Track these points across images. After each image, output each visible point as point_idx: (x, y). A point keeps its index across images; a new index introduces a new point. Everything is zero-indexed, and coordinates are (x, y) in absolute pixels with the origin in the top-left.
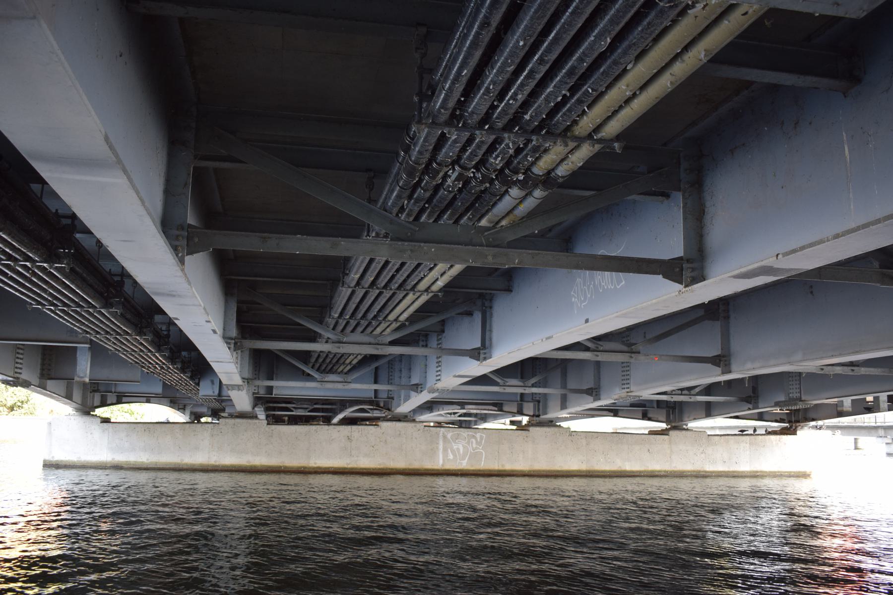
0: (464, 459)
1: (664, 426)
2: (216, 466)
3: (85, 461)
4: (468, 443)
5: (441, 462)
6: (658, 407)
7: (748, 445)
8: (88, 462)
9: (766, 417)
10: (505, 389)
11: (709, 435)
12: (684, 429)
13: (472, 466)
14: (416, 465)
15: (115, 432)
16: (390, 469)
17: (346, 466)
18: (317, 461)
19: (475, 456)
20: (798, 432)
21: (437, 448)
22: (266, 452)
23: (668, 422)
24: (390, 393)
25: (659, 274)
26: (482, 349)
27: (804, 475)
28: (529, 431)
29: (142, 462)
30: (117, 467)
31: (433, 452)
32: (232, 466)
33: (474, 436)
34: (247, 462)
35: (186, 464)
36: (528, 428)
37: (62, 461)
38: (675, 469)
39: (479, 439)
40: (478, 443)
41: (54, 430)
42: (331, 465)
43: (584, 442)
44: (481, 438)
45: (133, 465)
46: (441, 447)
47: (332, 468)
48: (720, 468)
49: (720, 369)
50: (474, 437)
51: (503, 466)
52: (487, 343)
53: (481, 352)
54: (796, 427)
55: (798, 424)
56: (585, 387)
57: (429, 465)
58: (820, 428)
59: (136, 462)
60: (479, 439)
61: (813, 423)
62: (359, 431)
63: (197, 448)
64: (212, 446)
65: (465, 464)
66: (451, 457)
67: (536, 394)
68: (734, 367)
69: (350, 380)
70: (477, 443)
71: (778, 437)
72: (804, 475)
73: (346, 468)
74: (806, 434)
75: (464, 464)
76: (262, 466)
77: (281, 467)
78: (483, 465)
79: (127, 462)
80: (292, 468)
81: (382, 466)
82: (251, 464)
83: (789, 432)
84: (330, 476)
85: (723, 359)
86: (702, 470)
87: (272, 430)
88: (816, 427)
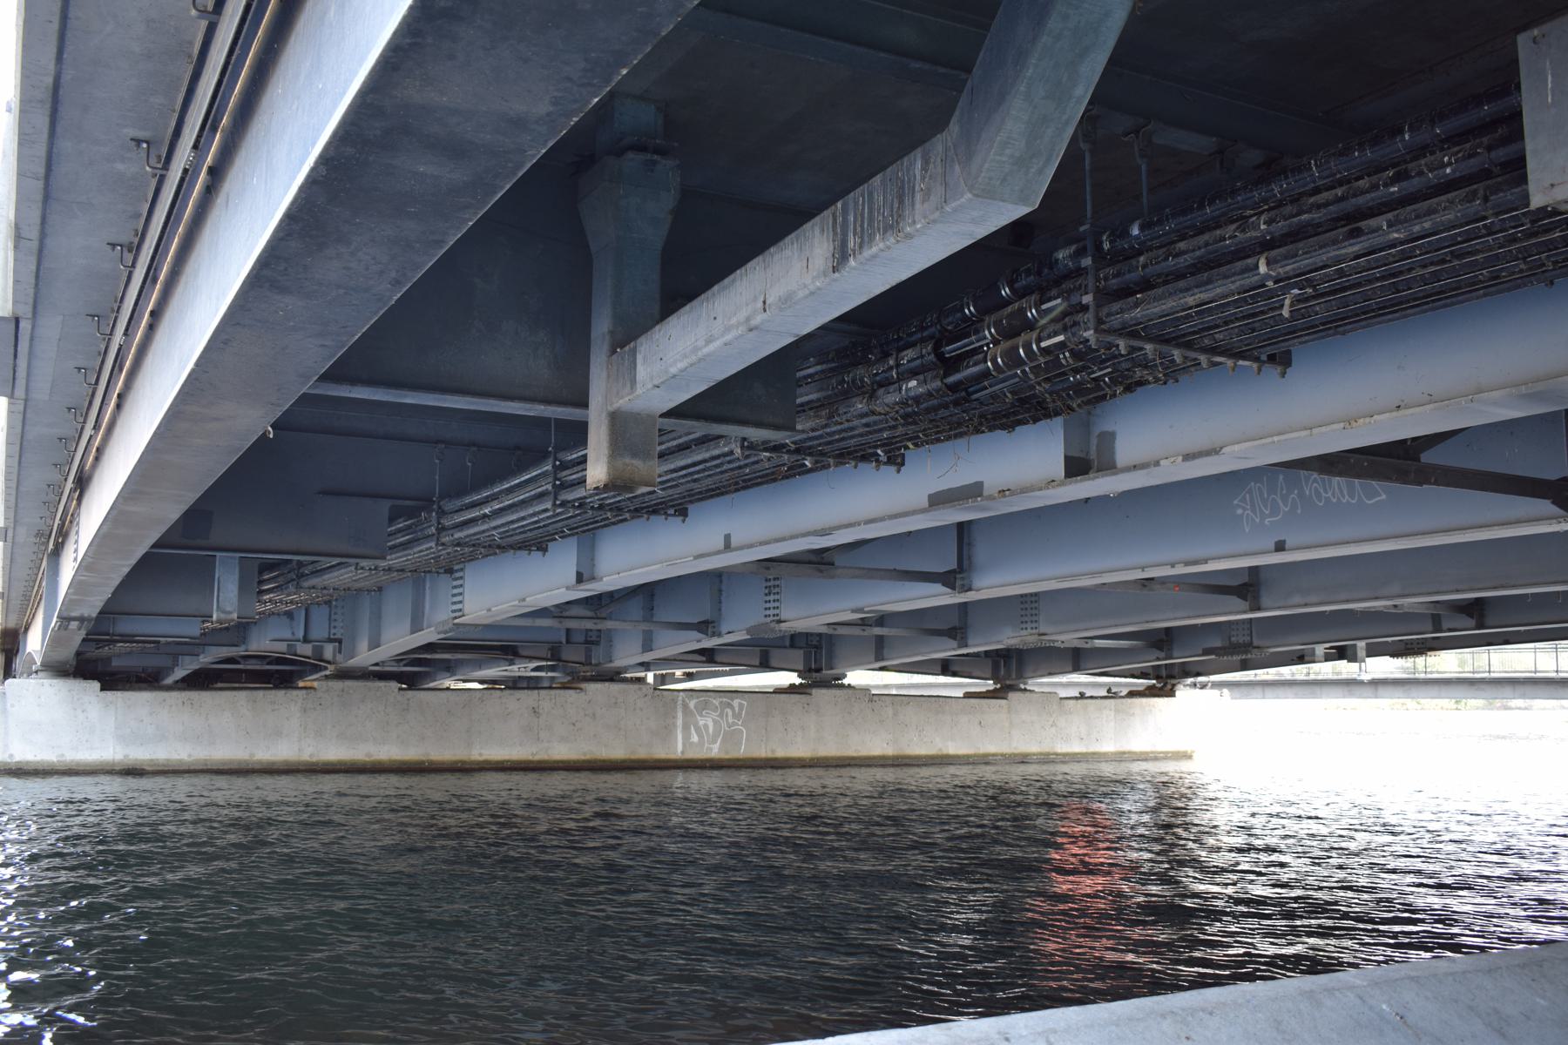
0: (714, 742)
1: (990, 685)
2: (313, 764)
3: (72, 761)
4: (721, 715)
5: (680, 747)
6: (792, 646)
7: (1112, 713)
8: (78, 764)
9: (718, 658)
10: (835, 629)
11: (1061, 699)
12: (1021, 690)
13: (727, 753)
14: (642, 753)
15: (129, 707)
16: (600, 761)
17: (531, 758)
18: (483, 751)
19: (731, 737)
20: (1177, 693)
21: (675, 725)
22: (398, 737)
23: (995, 678)
24: (590, 633)
25: (1548, 499)
26: (960, 573)
27: (1186, 756)
28: (810, 694)
29: (180, 761)
30: (132, 771)
31: (667, 732)
32: (340, 763)
33: (729, 704)
34: (367, 755)
35: (260, 762)
36: (808, 691)
37: (28, 762)
38: (1016, 751)
39: (737, 709)
40: (737, 716)
41: (12, 706)
42: (507, 758)
43: (890, 711)
44: (741, 706)
45: (164, 765)
46: (680, 722)
47: (508, 761)
48: (1077, 748)
49: (1248, 603)
50: (730, 706)
51: (773, 751)
52: (966, 563)
53: (958, 576)
54: (1174, 685)
55: (1174, 681)
56: (945, 627)
57: (661, 753)
58: (1203, 686)
59: (168, 760)
60: (737, 709)
61: (1190, 680)
62: (551, 699)
63: (278, 733)
64: (305, 728)
65: (717, 750)
66: (695, 738)
67: (591, 630)
68: (1265, 600)
69: (604, 615)
70: (734, 716)
71: (1144, 700)
72: (1186, 756)
73: (531, 762)
74: (1186, 694)
75: (715, 751)
76: (391, 761)
77: (423, 762)
78: (743, 751)
79: (152, 760)
80: (443, 763)
81: (588, 757)
82: (372, 759)
83: (1162, 693)
84: (563, 774)
85: (1251, 589)
86: (1052, 751)
87: (408, 700)
88: (1195, 685)
